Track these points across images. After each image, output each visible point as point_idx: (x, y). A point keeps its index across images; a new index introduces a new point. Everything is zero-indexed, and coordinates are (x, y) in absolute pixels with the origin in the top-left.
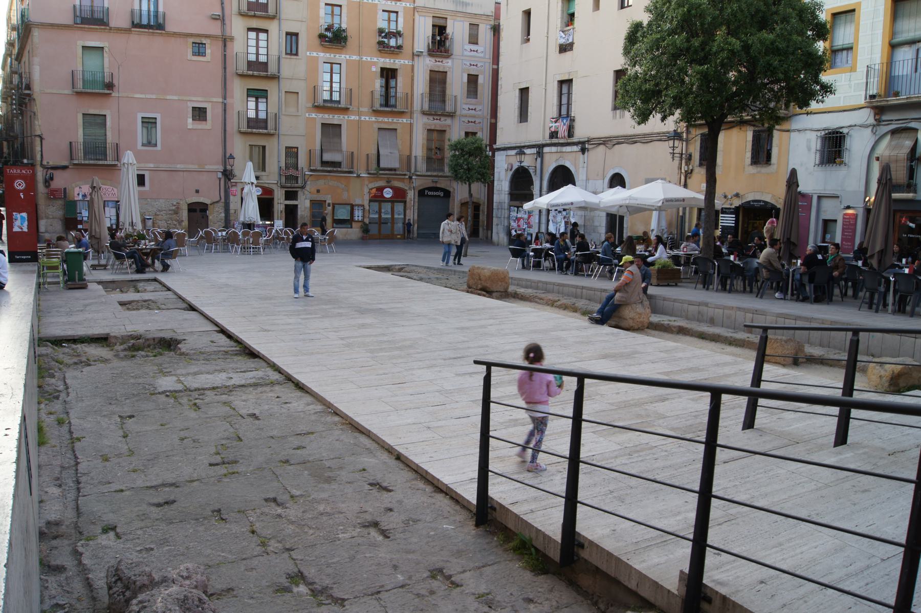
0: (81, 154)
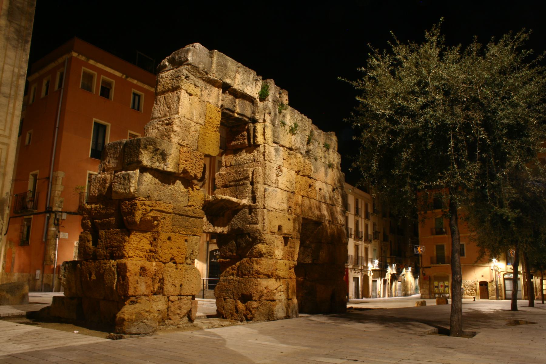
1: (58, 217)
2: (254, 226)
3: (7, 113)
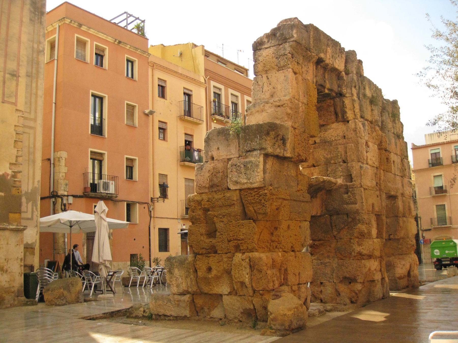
0: (436, 223)
1: (65, 202)
2: (353, 206)
3: (31, 94)
